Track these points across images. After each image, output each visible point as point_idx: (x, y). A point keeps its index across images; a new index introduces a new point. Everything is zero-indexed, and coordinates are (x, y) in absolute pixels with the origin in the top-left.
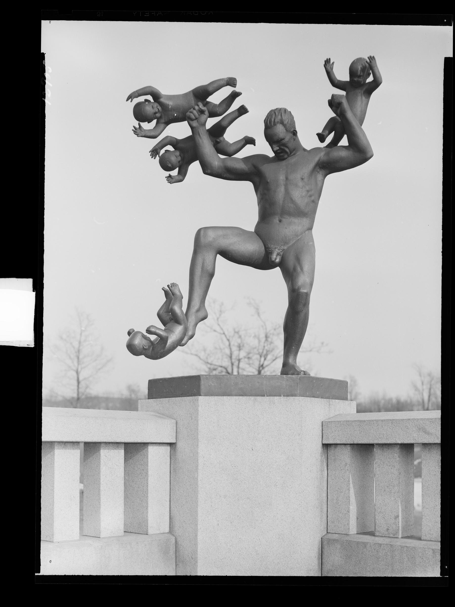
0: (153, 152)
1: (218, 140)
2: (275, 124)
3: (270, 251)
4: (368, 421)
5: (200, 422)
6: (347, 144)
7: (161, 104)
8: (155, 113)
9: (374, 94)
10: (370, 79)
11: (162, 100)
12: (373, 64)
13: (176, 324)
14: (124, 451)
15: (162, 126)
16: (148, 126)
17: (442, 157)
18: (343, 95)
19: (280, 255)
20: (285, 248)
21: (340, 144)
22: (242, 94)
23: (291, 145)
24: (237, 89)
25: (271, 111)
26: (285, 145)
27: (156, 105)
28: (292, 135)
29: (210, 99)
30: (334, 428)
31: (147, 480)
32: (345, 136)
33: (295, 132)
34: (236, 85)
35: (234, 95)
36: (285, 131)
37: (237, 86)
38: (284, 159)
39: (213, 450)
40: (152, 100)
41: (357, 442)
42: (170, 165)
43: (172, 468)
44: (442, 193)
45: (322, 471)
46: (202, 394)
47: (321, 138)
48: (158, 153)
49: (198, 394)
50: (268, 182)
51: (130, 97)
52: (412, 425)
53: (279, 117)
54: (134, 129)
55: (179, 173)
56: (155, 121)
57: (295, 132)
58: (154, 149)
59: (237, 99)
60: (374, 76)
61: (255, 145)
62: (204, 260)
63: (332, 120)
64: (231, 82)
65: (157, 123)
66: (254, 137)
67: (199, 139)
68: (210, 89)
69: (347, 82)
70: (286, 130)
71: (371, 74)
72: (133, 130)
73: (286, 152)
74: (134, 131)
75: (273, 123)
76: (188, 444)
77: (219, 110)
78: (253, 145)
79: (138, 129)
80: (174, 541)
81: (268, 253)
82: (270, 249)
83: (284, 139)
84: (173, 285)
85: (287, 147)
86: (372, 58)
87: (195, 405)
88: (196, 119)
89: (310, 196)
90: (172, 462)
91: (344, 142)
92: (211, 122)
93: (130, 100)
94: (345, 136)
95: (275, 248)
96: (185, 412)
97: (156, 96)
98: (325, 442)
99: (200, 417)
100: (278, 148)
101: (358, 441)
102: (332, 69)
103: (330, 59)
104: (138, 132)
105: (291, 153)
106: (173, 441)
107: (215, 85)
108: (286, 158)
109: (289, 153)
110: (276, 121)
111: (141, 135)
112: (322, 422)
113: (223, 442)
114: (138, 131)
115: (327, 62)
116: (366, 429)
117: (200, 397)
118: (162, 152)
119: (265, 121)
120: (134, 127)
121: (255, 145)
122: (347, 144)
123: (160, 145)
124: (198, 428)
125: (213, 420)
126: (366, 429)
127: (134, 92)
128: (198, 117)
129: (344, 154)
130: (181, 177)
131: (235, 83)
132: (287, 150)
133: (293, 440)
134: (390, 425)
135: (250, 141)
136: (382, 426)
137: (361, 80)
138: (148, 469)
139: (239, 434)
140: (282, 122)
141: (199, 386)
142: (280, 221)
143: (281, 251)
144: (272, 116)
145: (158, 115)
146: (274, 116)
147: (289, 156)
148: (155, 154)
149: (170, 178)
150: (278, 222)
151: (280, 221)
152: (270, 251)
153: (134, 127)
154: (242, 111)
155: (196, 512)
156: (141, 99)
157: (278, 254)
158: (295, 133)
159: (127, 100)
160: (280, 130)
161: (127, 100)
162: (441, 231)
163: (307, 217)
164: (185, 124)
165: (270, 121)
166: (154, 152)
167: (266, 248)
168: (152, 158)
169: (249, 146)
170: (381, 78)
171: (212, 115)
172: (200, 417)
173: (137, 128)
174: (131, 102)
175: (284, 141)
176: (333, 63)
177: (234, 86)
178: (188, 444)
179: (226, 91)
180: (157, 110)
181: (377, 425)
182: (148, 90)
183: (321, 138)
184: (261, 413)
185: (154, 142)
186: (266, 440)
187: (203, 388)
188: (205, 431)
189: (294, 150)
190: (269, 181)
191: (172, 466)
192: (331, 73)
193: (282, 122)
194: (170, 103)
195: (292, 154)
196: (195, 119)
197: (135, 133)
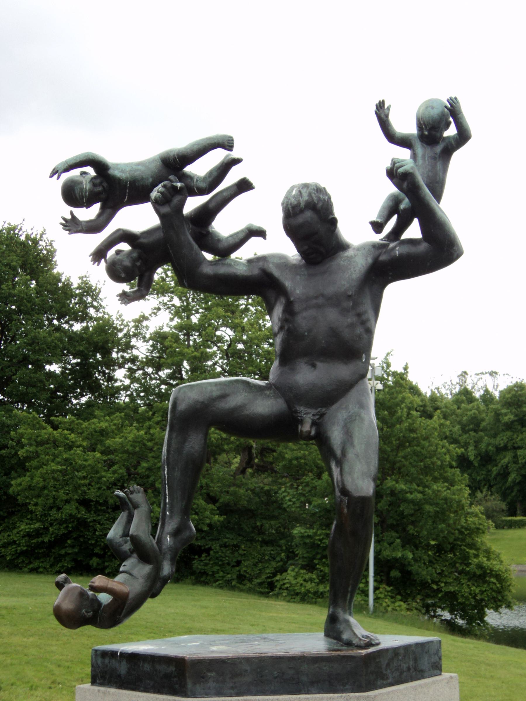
9: (457, 156)
24: (235, 154)
32: (416, 221)
37: (235, 148)
47: (377, 227)
51: (55, 172)
54: (64, 222)
61: (265, 238)
71: (450, 123)
72: (61, 224)
78: (261, 239)
93: (56, 176)
94: (416, 221)
102: (387, 116)
103: (383, 101)
118: (111, 253)
121: (265, 238)
135: (261, 233)
153: (64, 219)
156: (75, 173)
159: (51, 176)
161: (51, 176)
169: (254, 241)
174: (58, 178)
176: (389, 108)
183: (377, 227)
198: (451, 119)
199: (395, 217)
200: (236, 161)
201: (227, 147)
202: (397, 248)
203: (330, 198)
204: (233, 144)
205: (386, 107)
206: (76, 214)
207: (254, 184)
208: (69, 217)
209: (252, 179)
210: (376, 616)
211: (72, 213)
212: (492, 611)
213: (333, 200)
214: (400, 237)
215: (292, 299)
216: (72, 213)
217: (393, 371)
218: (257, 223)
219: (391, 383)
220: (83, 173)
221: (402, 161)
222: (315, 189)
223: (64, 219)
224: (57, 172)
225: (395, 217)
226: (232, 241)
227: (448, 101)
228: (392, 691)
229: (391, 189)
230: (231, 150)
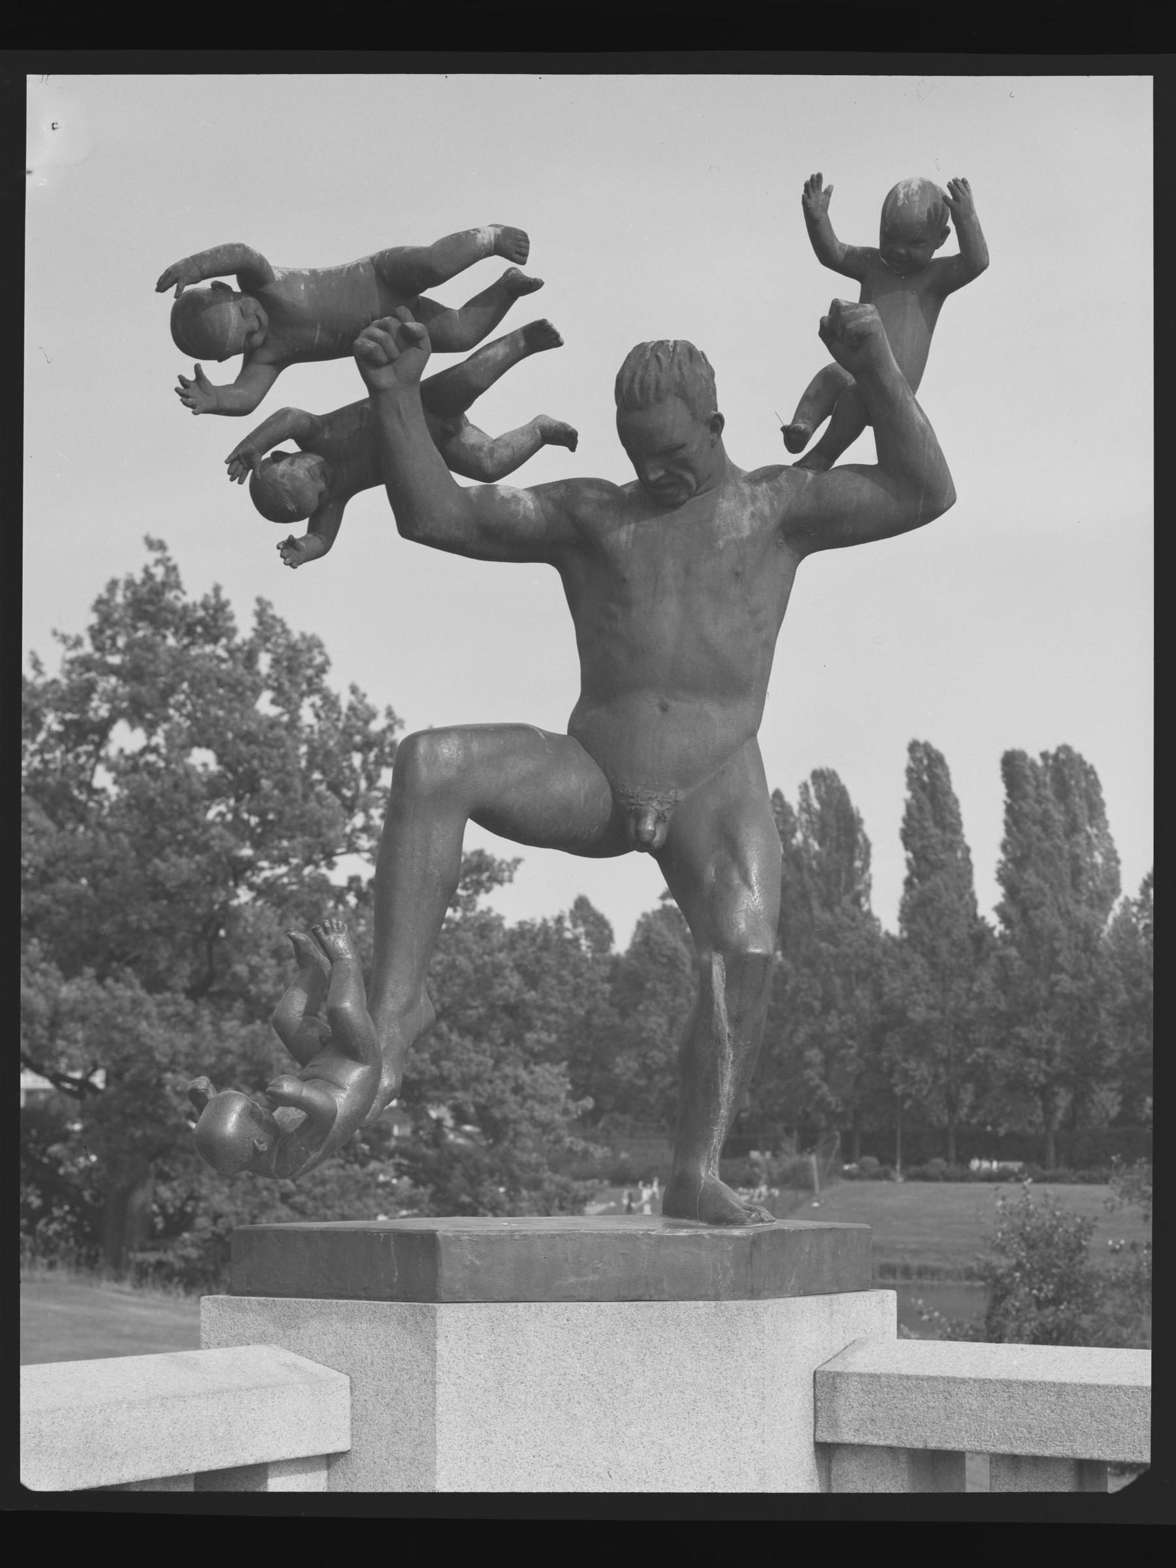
0: (237, 463)
2: (659, 399)
3: (633, 808)
4: (975, 1381)
6: (872, 460)
7: (271, 304)
10: (950, 248)
13: (349, 1062)
15: (264, 371)
19: (665, 821)
20: (682, 795)
21: (848, 457)
22: (543, 284)
24: (528, 270)
25: (641, 349)
26: (685, 464)
27: (252, 303)
28: (709, 430)
29: (430, 294)
30: (856, 1394)
32: (868, 432)
33: (719, 422)
34: (526, 255)
36: (690, 418)
37: (530, 259)
38: (675, 505)
39: (483, 1480)
40: (236, 288)
41: (939, 1445)
42: (291, 507)
46: (444, 1296)
49: (434, 1297)
50: (624, 580)
52: (1128, 1405)
54: (181, 387)
55: (311, 529)
57: (719, 422)
58: (240, 452)
61: (573, 449)
63: (825, 377)
66: (574, 425)
69: (869, 251)
70: (693, 415)
71: (948, 231)
72: (177, 390)
73: (687, 484)
74: (181, 394)
75: (652, 392)
76: (397, 1459)
77: (461, 330)
78: (564, 450)
79: (193, 385)
82: (631, 800)
83: (683, 446)
84: (332, 927)
85: (692, 470)
87: (421, 1331)
88: (391, 361)
92: (438, 363)
94: (868, 432)
95: (650, 799)
96: (382, 1353)
99: (441, 1373)
100: (661, 473)
101: (939, 1442)
102: (825, 208)
105: (698, 487)
108: (684, 502)
109: (694, 487)
110: (663, 385)
112: (815, 1372)
113: (516, 1454)
114: (194, 391)
115: (814, 184)
116: (968, 1406)
117: (448, 1315)
120: (182, 379)
121: (573, 449)
122: (872, 460)
124: (434, 1409)
125: (483, 1382)
126: (968, 1406)
128: (395, 356)
129: (867, 492)
130: (317, 542)
131: (524, 250)
132: (689, 477)
133: (736, 1442)
134: (1053, 1399)
135: (566, 437)
136: (1025, 1402)
137: (918, 253)
139: (567, 1427)
142: (664, 708)
143: (668, 806)
147: (691, 495)
148: (244, 468)
149: (291, 550)
150: (658, 711)
151: (664, 708)
152: (633, 808)
153: (182, 379)
159: (162, 287)
164: (347, 366)
165: (641, 383)
167: (618, 796)
168: (232, 479)
171: (442, 345)
172: (441, 1373)
173: (190, 382)
175: (683, 453)
176: (828, 193)
177: (521, 258)
178: (397, 1459)
180: (256, 324)
181: (1006, 1395)
184: (635, 1357)
185: (239, 429)
186: (653, 1443)
187: (450, 1274)
188: (458, 1419)
190: (627, 575)
194: (300, 296)
195: (703, 488)
196: (387, 364)
197: (184, 399)
198: (950, 224)
199: (829, 418)
200: (533, 286)
201: (517, 256)
202: (331, 506)
203: (712, 375)
204: (528, 248)
205: (824, 187)
207: (563, 336)
208: (191, 376)
211: (198, 369)
213: (718, 380)
216: (198, 369)
218: (560, 415)
219: (655, 1188)
220: (218, 286)
221: (851, 309)
225: (829, 418)
226: (504, 454)
227: (950, 187)
228: (830, 1230)
230: (523, 263)
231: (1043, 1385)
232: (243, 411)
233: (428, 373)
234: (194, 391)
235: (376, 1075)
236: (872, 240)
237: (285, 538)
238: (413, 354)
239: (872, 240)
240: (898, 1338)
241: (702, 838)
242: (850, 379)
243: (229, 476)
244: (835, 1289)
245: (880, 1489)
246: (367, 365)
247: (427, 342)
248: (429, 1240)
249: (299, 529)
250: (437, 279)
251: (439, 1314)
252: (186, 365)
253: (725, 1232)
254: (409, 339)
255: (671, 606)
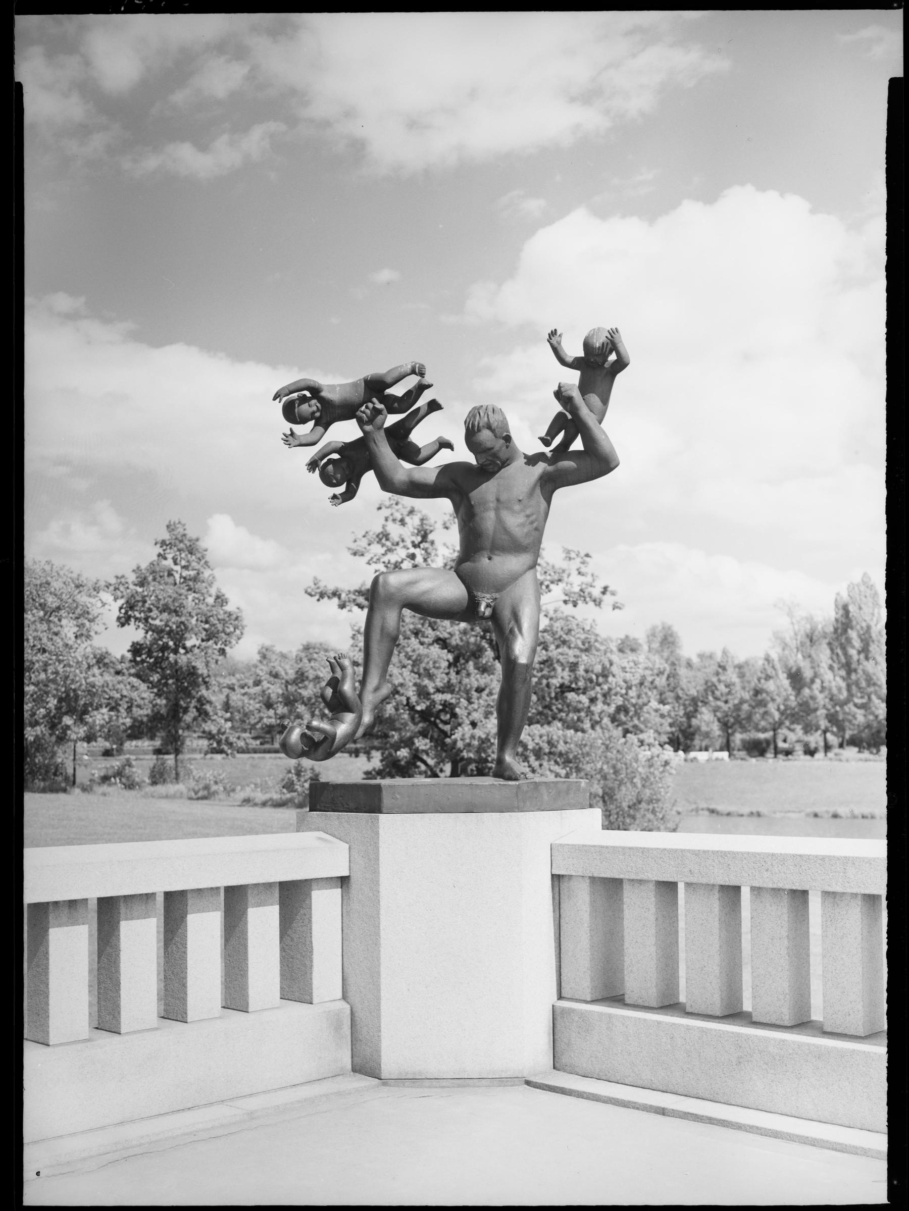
1: (402, 445)
2: (479, 430)
5: (381, 850)
7: (322, 400)
8: (313, 413)
10: (613, 357)
11: (323, 394)
12: (617, 341)
14: (277, 908)
16: (304, 430)
17: (885, 294)
18: (574, 385)
23: (503, 455)
29: (389, 391)
31: (311, 929)
35: (421, 388)
43: (344, 910)
44: (885, 161)
45: (554, 911)
47: (546, 442)
48: (317, 466)
53: (486, 419)
56: (311, 424)
59: (426, 392)
60: (618, 354)
61: (453, 450)
62: (384, 619)
63: (560, 416)
64: (418, 371)
65: (315, 425)
67: (375, 447)
68: (389, 380)
69: (582, 357)
70: (496, 436)
75: (476, 428)
78: (449, 450)
80: (349, 1012)
81: (473, 603)
83: (493, 448)
86: (613, 333)
89: (532, 523)
90: (345, 902)
91: (578, 445)
92: (392, 419)
93: (278, 399)
97: (315, 391)
98: (556, 872)
100: (484, 460)
103: (555, 330)
104: (290, 439)
106: (346, 873)
107: (395, 375)
110: (481, 425)
111: (294, 444)
117: (382, 817)
119: (465, 422)
121: (453, 450)
123: (320, 454)
127: (283, 389)
135: (445, 444)
138: (311, 914)
140: (489, 427)
141: (380, 800)
144: (474, 416)
145: (318, 414)
146: (478, 418)
150: (488, 561)
153: (285, 435)
154: (434, 406)
155: (379, 973)
157: (488, 606)
158: (508, 439)
159: (275, 399)
160: (485, 436)
161: (275, 399)
162: (885, 312)
163: (527, 552)
166: (313, 465)
169: (445, 451)
170: (628, 357)
171: (392, 411)
179: (411, 382)
182: (302, 385)
185: (311, 452)
189: (507, 460)
191: (344, 907)
192: (559, 349)
193: (489, 427)
200: (429, 386)
206: (295, 431)
209: (441, 401)
210: (654, 635)
211: (291, 430)
212: (672, 749)
214: (569, 448)
215: (473, 503)
216: (291, 430)
217: (168, 534)
222: (794, 670)
223: (285, 435)
224: (279, 396)
229: (558, 408)
231: (637, 848)
232: (313, 444)
233: (387, 425)
234: (290, 438)
235: (360, 718)
236: (581, 353)
237: (332, 495)
238: (380, 417)
239: (581, 353)
240: (606, 827)
241: (506, 614)
242: (569, 417)
243: (135, 568)
244: (352, 805)
245: (885, 928)
246: (361, 423)
247: (385, 411)
248: (378, 788)
249: (342, 489)
250: (390, 386)
251: (380, 818)
252: (287, 426)
253: (510, 783)
254: (377, 412)
255: (491, 515)
